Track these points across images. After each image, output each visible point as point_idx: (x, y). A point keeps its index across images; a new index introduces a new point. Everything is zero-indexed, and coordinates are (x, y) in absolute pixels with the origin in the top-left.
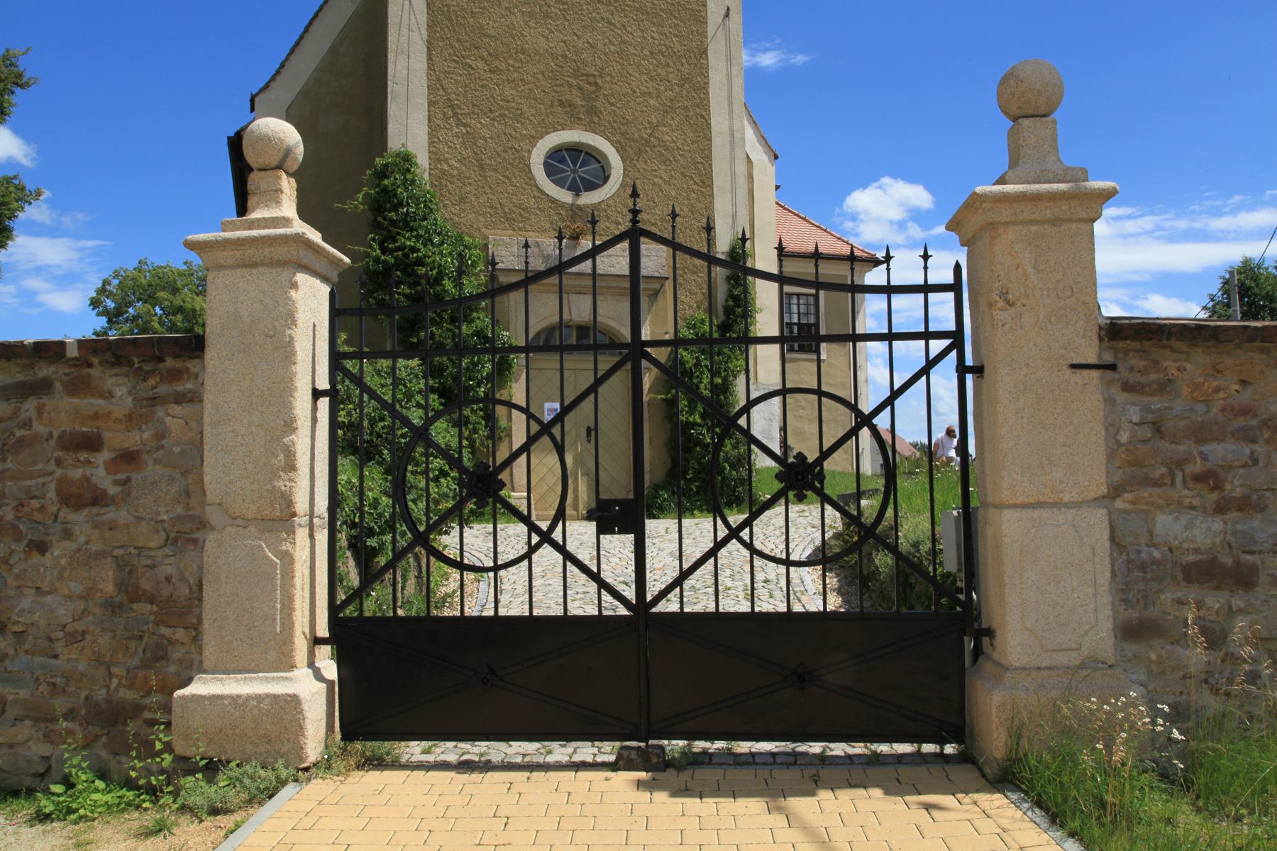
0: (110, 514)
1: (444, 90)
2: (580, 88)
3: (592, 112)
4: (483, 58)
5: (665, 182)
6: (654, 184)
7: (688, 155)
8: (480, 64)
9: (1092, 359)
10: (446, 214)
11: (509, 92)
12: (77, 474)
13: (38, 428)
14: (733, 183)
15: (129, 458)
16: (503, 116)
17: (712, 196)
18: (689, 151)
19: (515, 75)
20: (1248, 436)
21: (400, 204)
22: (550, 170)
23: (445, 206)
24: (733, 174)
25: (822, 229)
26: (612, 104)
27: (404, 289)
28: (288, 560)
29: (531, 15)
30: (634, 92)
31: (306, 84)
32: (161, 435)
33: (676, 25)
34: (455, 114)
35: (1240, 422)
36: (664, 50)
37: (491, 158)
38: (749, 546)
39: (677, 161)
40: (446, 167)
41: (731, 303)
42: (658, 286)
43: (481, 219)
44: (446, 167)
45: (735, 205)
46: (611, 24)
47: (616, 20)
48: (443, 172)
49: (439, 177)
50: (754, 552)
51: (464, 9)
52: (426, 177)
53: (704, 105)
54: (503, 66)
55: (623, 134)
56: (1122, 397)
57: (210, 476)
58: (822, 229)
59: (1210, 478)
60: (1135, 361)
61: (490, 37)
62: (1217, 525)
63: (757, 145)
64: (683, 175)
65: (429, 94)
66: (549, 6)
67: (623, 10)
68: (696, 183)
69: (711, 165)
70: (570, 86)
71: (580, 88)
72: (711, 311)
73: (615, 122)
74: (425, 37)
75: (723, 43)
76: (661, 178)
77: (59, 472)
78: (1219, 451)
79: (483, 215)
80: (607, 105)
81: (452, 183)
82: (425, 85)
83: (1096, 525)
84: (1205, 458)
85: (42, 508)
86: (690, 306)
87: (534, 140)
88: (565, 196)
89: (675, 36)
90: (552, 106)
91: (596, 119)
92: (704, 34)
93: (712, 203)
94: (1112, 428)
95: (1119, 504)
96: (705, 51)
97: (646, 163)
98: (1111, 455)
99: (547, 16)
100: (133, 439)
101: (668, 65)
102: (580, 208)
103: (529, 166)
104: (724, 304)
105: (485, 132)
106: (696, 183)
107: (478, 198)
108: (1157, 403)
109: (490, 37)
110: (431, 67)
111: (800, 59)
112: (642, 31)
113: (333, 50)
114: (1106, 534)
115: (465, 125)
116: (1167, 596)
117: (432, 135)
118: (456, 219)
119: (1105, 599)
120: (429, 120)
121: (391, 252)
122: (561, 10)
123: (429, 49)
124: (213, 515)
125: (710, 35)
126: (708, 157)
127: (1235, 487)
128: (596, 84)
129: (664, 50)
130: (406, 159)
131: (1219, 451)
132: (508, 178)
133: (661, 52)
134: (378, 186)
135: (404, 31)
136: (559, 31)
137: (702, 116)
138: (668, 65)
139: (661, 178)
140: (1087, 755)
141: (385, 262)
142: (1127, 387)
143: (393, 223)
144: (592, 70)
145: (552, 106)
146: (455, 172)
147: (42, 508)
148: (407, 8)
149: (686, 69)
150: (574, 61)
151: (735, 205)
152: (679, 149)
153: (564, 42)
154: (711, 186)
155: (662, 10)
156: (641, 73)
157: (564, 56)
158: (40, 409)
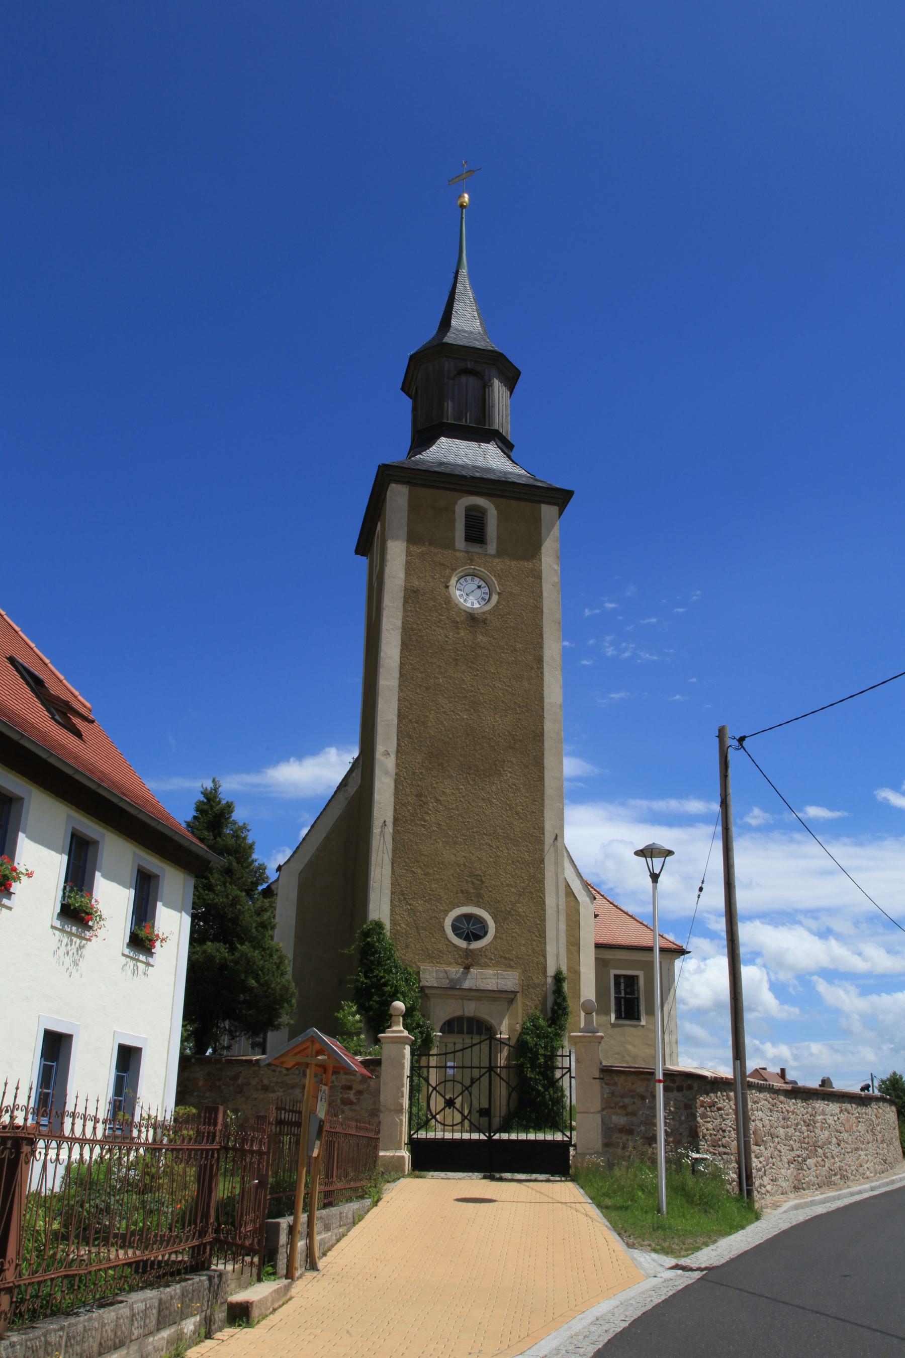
0: (354, 1107)
1: (399, 885)
2: (473, 883)
3: (479, 896)
4: (421, 867)
5: (519, 935)
6: (512, 937)
7: (532, 920)
8: (419, 871)
9: (598, 1077)
10: (399, 954)
12: (346, 1096)
13: (336, 1083)
14: (557, 935)
15: (360, 1093)
16: (430, 899)
17: (545, 944)
18: (533, 917)
19: (438, 876)
20: (633, 1097)
21: (376, 952)
22: (455, 928)
23: (398, 950)
24: (558, 930)
25: (644, 925)
26: (490, 892)
27: (376, 998)
28: (401, 1120)
29: (448, 843)
30: (502, 884)
31: (311, 858)
32: (368, 1086)
33: (527, 846)
34: (405, 899)
35: (631, 1094)
36: (520, 859)
37: (423, 923)
38: (463, 1085)
39: (525, 923)
40: (399, 928)
41: (556, 1008)
42: (513, 996)
43: (417, 957)
44: (399, 928)
45: (558, 948)
46: (491, 846)
47: (493, 844)
48: (397, 931)
49: (395, 933)
50: (462, 1084)
51: (412, 841)
52: (388, 934)
53: (541, 891)
54: (431, 871)
55: (496, 908)
56: (605, 1086)
57: (382, 1098)
58: (644, 925)
59: (624, 1107)
60: (609, 1078)
61: (425, 855)
62: (625, 1119)
63: (583, 891)
64: (529, 931)
65: (392, 888)
66: (457, 838)
67: (497, 838)
68: (536, 936)
69: (545, 925)
70: (467, 882)
71: (473, 883)
72: (544, 1011)
73: (491, 901)
74: (391, 857)
75: (553, 855)
76: (516, 933)
77: (341, 1096)
78: (627, 1101)
79: (418, 954)
80: (487, 892)
81: (402, 937)
82: (390, 883)
83: (598, 1118)
84: (623, 1102)
85: (336, 1105)
86: (531, 1008)
87: (446, 912)
88: (462, 944)
89: (526, 851)
90: (457, 893)
91: (481, 900)
92: (542, 850)
93: (545, 947)
94: (602, 1094)
95: (604, 1113)
96: (543, 860)
97: (508, 924)
98: (602, 1101)
99: (456, 843)
100: (361, 1087)
101: (522, 868)
102: (471, 951)
103: (443, 927)
104: (551, 1006)
105: (420, 908)
106: (536, 936)
107: (415, 945)
108: (613, 1088)
109: (425, 855)
110: (393, 873)
112: (508, 849)
113: (327, 837)
114: (600, 1120)
115: (410, 905)
116: (614, 1137)
118: (403, 957)
119: (600, 1137)
120: (391, 902)
121: (371, 978)
122: (463, 840)
123: (393, 864)
124: (382, 1109)
125: (546, 850)
126: (543, 920)
127: (630, 1109)
128: (481, 880)
129: (520, 859)
130: (379, 925)
131: (627, 1101)
132: (431, 934)
133: (518, 861)
134: (364, 941)
135: (380, 854)
136: (462, 851)
137: (541, 897)
138: (522, 868)
139: (516, 933)
141: (366, 983)
142: (606, 1084)
143: (372, 962)
144: (479, 872)
145: (457, 893)
146: (404, 931)
147: (336, 1105)
148: (382, 841)
149: (532, 870)
150: (470, 868)
151: (558, 948)
152: (527, 916)
153: (465, 857)
154: (545, 938)
155: (519, 837)
156: (507, 873)
157: (465, 865)
158: (337, 1078)
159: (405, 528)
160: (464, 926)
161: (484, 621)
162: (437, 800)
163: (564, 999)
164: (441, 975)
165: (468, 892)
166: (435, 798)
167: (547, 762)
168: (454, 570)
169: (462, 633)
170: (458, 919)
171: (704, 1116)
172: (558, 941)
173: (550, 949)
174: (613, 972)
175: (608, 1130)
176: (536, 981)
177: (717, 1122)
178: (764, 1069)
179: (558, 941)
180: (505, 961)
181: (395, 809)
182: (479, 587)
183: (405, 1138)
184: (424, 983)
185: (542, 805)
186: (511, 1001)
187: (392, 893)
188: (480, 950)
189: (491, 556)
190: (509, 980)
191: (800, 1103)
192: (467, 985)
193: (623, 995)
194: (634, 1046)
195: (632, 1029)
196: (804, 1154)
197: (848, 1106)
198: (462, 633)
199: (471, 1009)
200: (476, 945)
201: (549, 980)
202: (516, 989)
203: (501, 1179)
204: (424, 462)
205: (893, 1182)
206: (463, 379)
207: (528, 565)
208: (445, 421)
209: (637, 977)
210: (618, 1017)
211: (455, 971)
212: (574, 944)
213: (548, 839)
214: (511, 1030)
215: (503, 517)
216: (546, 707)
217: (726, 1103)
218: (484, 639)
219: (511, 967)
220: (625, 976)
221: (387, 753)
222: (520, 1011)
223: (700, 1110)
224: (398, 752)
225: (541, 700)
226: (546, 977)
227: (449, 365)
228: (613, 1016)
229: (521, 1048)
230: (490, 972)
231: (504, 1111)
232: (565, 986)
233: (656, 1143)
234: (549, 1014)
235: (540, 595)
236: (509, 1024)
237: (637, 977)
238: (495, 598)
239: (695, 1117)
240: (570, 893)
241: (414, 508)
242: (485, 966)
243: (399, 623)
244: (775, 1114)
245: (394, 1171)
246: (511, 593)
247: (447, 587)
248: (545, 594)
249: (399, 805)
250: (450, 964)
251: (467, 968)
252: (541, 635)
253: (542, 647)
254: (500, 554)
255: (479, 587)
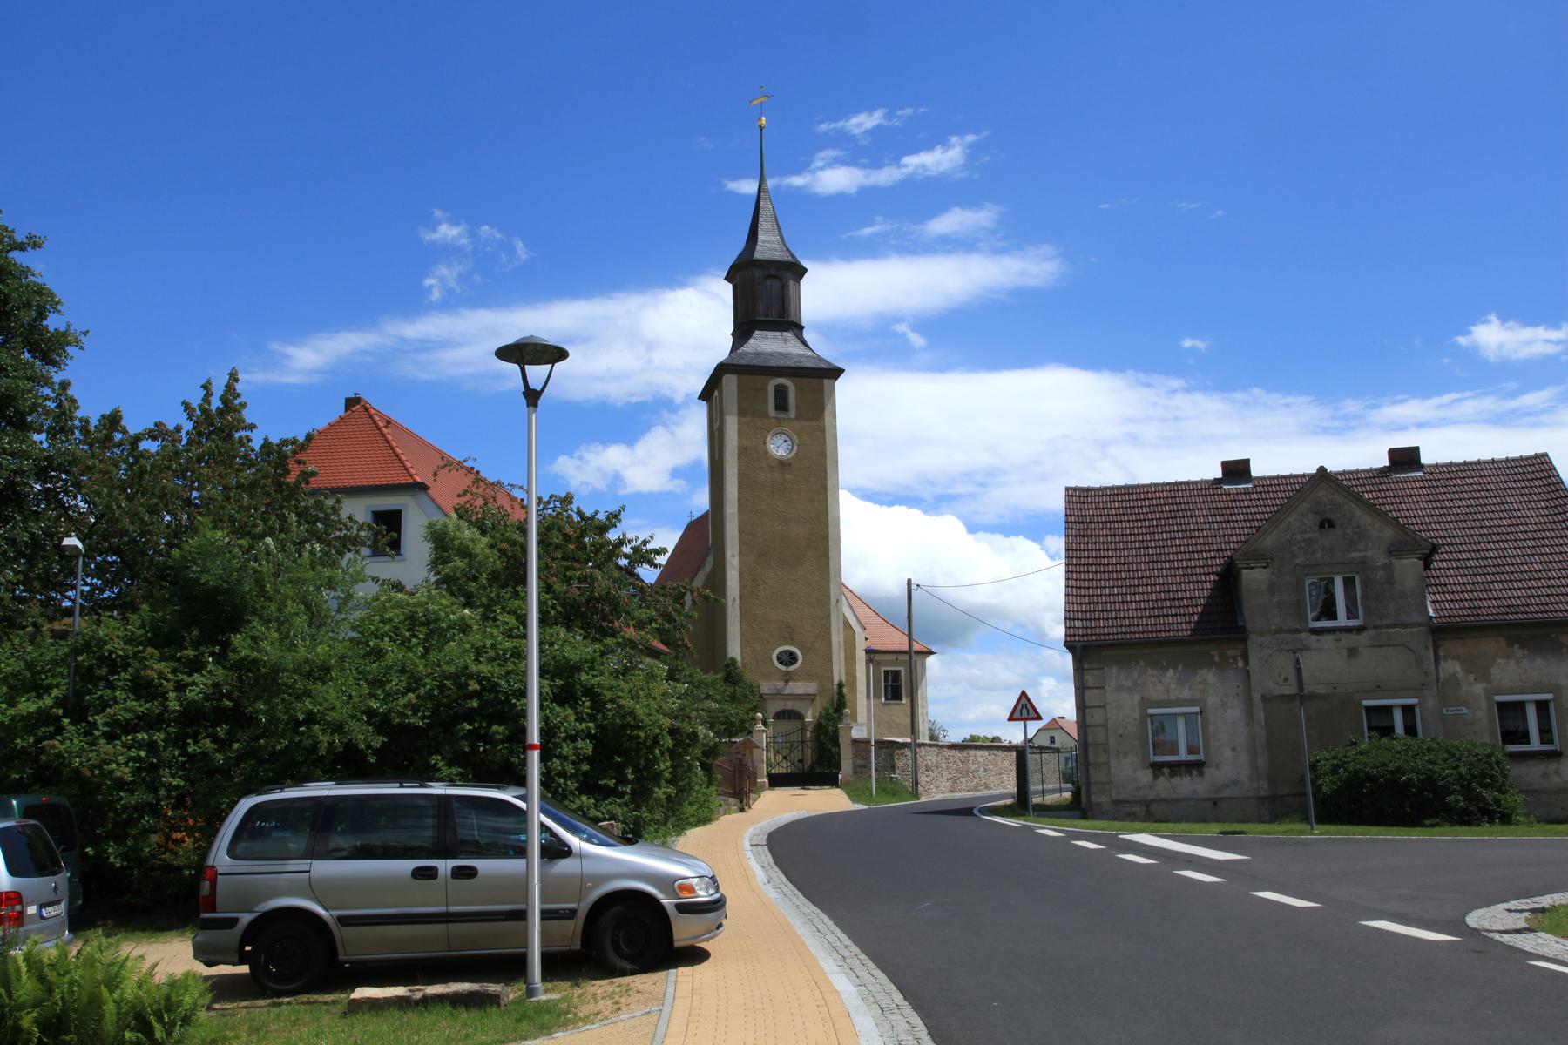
3: (792, 639)
11: (766, 635)
22: (778, 658)
24: (840, 658)
49: (743, 663)
53: (830, 634)
59: (862, 757)
72: (832, 704)
83: (851, 761)
87: (773, 650)
88: (783, 668)
92: (829, 609)
111: (985, 134)
117: (742, 652)
130: (733, 660)
131: (864, 754)
140: (158, 460)
159: (736, 405)
160: (784, 657)
161: (789, 465)
162: (765, 583)
163: (844, 697)
164: (772, 687)
165: (785, 638)
166: (764, 581)
167: (831, 554)
168: (769, 431)
169: (776, 474)
170: (781, 653)
171: (897, 759)
172: (839, 663)
173: (835, 668)
174: (883, 669)
175: (855, 766)
176: (827, 687)
177: (904, 762)
178: (1063, 718)
179: (839, 663)
180: (808, 676)
181: (740, 590)
182: (785, 441)
183: (765, 773)
184: (762, 692)
185: (829, 581)
186: (813, 700)
187: (741, 640)
188: (794, 671)
189: (792, 420)
190: (811, 687)
191: (958, 752)
192: (786, 692)
193: (890, 683)
194: (898, 717)
195: (897, 707)
196: (959, 776)
197: (996, 752)
198: (776, 474)
199: (790, 705)
200: (792, 668)
201: (835, 687)
202: (816, 692)
203: (808, 789)
204: (746, 354)
205: (1285, 832)
206: (768, 282)
207: (818, 423)
208: (758, 319)
209: (900, 671)
210: (886, 699)
211: (780, 684)
212: (850, 659)
213: (833, 601)
214: (813, 717)
215: (799, 392)
216: (830, 518)
217: (907, 752)
218: (790, 477)
219: (813, 680)
220: (892, 671)
221: (733, 556)
222: (818, 706)
223: (897, 757)
224: (739, 554)
225: (827, 514)
226: (833, 684)
227: (758, 273)
228: (883, 699)
229: (819, 727)
230: (800, 684)
231: (810, 762)
232: (845, 690)
233: (525, 697)
234: (835, 706)
235: (825, 444)
236: (813, 713)
237: (900, 671)
238: (796, 448)
239: (893, 760)
240: (847, 624)
241: (741, 390)
242: (797, 680)
243: (736, 471)
244: (940, 757)
245: (762, 788)
246: (806, 444)
247: (765, 443)
248: (828, 443)
249: (742, 587)
250: (776, 680)
251: (787, 682)
252: (826, 473)
253: (826, 480)
254: (798, 418)
255: (785, 441)
